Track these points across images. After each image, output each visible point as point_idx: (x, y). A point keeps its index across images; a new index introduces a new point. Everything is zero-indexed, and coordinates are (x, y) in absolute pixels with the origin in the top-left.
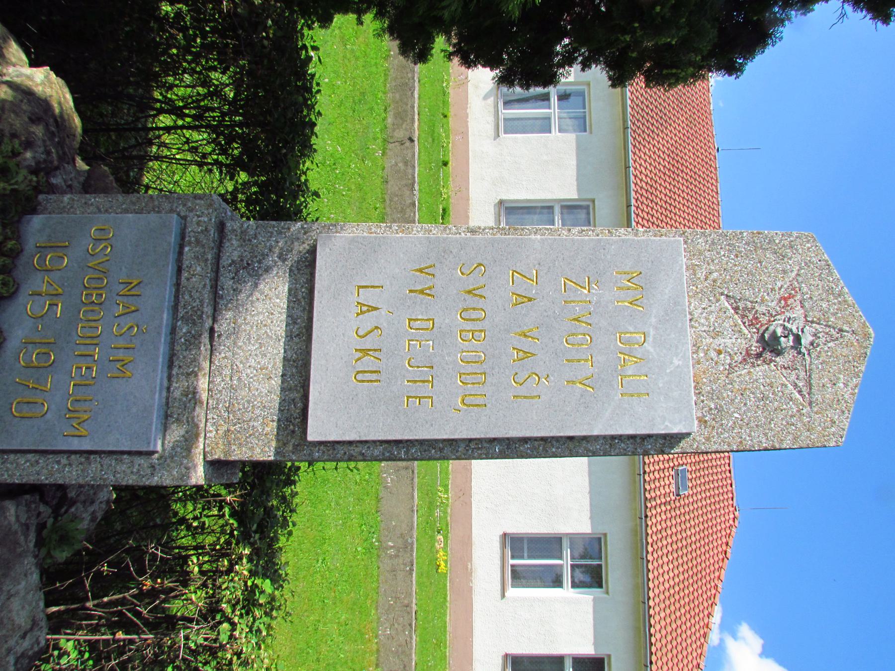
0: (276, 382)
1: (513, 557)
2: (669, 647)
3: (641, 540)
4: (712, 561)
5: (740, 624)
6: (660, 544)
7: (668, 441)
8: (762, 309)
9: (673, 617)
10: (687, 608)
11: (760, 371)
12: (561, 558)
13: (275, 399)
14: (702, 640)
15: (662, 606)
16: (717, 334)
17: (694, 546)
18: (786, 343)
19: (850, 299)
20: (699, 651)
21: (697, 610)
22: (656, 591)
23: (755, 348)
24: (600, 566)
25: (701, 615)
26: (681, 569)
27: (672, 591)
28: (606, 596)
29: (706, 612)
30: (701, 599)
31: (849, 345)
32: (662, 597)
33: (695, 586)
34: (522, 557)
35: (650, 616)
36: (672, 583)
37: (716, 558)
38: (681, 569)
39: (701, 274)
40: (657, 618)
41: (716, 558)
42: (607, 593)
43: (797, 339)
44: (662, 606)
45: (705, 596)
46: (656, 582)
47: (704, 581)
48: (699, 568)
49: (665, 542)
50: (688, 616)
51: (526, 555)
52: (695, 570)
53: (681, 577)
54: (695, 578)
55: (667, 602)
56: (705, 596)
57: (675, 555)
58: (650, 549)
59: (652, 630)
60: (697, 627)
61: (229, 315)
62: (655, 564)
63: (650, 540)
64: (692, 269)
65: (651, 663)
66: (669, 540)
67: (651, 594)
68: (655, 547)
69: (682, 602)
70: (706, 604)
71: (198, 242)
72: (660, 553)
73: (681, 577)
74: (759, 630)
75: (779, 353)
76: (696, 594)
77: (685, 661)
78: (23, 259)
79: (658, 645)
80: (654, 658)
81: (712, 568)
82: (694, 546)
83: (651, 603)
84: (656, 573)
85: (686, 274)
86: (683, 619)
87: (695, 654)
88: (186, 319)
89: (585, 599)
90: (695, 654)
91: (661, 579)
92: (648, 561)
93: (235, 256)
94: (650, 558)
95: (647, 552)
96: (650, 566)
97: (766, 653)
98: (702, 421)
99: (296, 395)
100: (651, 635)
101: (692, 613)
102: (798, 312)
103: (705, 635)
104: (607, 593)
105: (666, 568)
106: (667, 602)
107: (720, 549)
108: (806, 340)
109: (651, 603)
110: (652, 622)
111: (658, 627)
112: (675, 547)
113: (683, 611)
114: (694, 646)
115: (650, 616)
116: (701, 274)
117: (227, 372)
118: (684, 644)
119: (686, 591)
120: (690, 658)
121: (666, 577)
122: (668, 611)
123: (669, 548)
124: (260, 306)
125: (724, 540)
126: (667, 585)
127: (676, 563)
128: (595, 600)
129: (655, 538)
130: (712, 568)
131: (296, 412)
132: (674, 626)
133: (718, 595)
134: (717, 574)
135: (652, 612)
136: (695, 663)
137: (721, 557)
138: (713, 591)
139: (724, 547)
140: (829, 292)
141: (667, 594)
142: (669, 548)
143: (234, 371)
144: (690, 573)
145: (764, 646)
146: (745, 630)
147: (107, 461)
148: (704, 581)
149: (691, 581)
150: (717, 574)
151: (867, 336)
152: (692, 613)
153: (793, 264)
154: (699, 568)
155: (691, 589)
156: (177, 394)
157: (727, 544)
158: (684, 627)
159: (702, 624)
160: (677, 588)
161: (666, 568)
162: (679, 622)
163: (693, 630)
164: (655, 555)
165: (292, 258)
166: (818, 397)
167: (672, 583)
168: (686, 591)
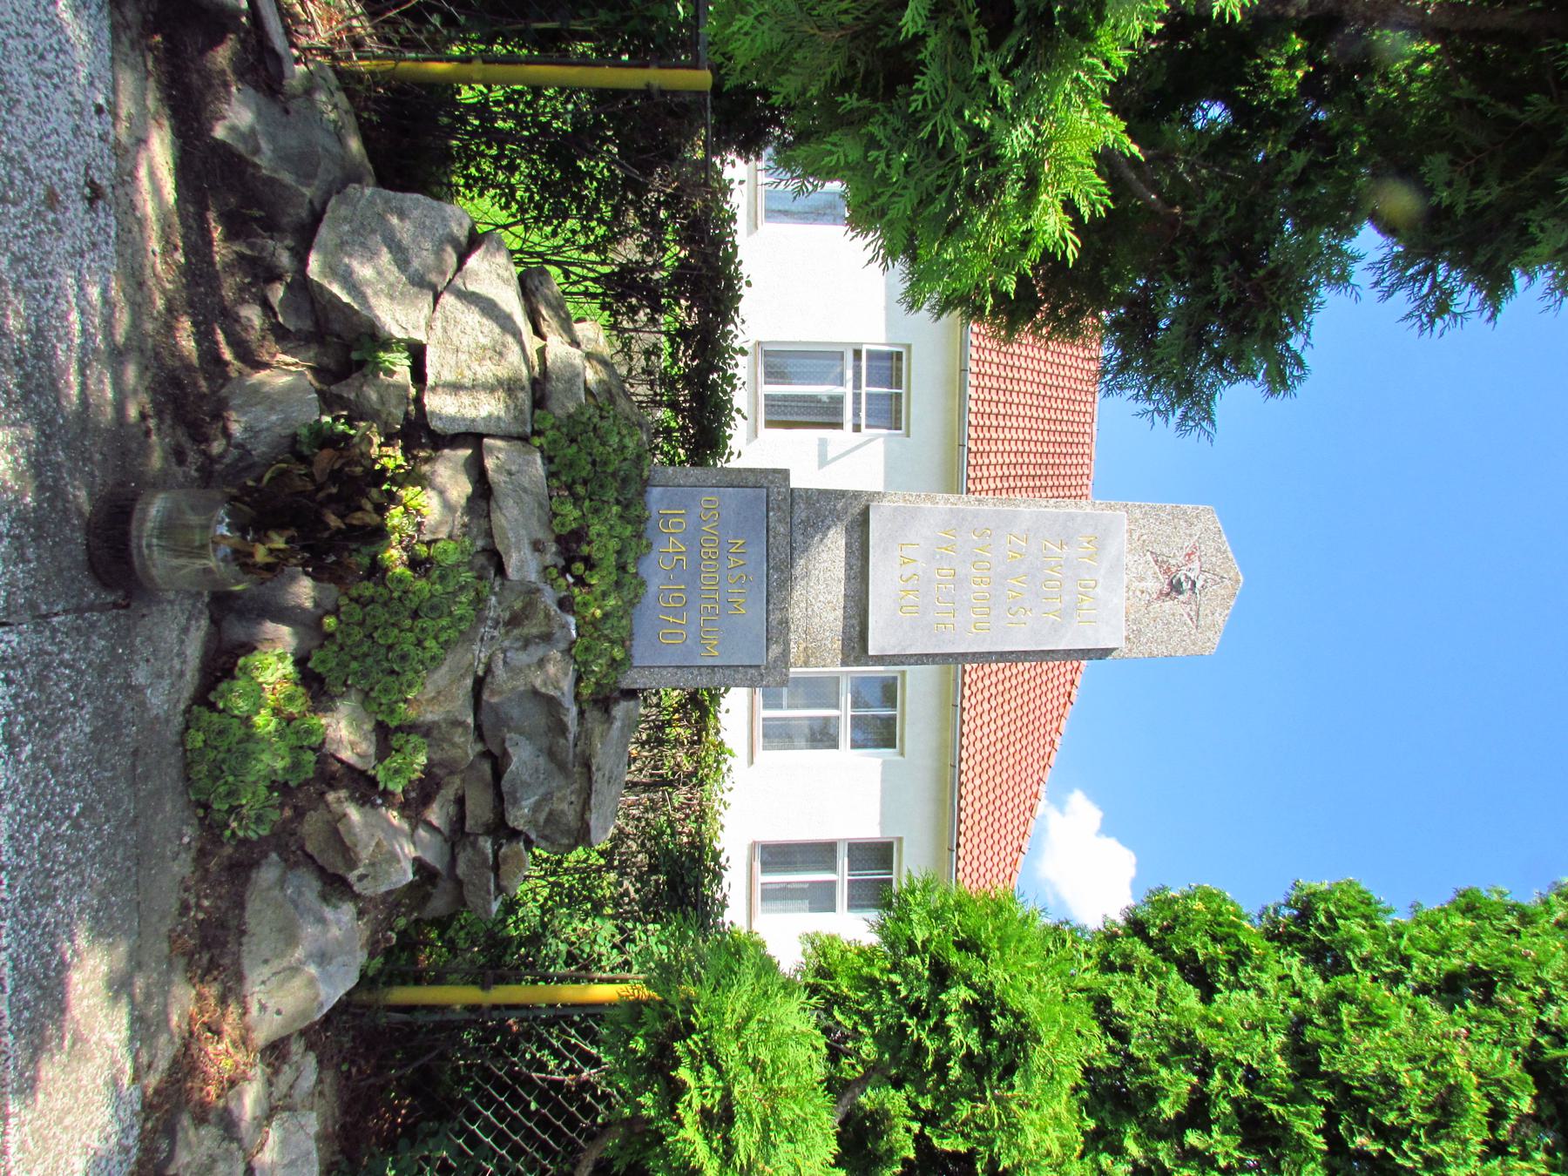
0: (840, 613)
1: (766, 707)
2: (983, 824)
3: (955, 680)
4: (1049, 707)
5: (1071, 791)
6: (980, 685)
7: (1104, 653)
8: (1173, 562)
9: (991, 784)
10: (1011, 772)
11: (1168, 604)
12: (837, 706)
13: (839, 625)
14: (1028, 814)
15: (978, 770)
16: (1142, 579)
17: (1026, 687)
18: (1186, 586)
19: (1231, 555)
20: (1022, 829)
21: (1024, 775)
22: (971, 750)
23: (1166, 589)
24: (893, 718)
25: (1029, 781)
26: (1006, 719)
27: (992, 750)
28: (899, 758)
29: (1036, 778)
30: (1030, 760)
31: (1226, 587)
32: (978, 758)
33: (1024, 742)
34: (780, 706)
35: (961, 784)
36: (993, 738)
37: (1056, 703)
38: (1006, 719)
39: (1135, 537)
40: (970, 786)
41: (1056, 703)
42: (902, 754)
43: (1194, 584)
44: (978, 770)
45: (1036, 756)
46: (972, 738)
47: (1036, 734)
48: (1031, 717)
49: (987, 682)
50: (1011, 783)
51: (862, 712)
52: (1025, 720)
53: (1006, 730)
54: (1025, 731)
55: (985, 765)
56: (1036, 756)
57: (1000, 700)
58: (967, 693)
59: (963, 803)
60: (1022, 797)
61: (802, 562)
62: (973, 713)
63: (967, 680)
64: (1131, 532)
65: (958, 845)
66: (994, 679)
67: (964, 755)
68: (974, 689)
69: (1005, 765)
70: (1036, 766)
71: (779, 508)
72: (980, 697)
73: (1006, 730)
74: (1095, 796)
75: (1180, 593)
76: (1024, 753)
77: (1003, 843)
78: (650, 524)
79: (969, 822)
80: (962, 840)
81: (1049, 717)
82: (1026, 687)
83: (964, 766)
84: (972, 725)
85: (1126, 536)
86: (1005, 787)
87: (1016, 833)
88: (777, 569)
89: (872, 761)
90: (1016, 833)
91: (979, 734)
92: (963, 709)
93: (804, 515)
94: (966, 704)
95: (963, 696)
96: (966, 717)
97: (1107, 829)
98: (1127, 638)
99: (855, 622)
100: (960, 809)
101: (1017, 779)
102: (1196, 565)
103: (1031, 809)
104: (902, 754)
105: (986, 718)
106: (985, 765)
107: (1062, 690)
108: (1198, 585)
109: (964, 766)
110: (963, 792)
111: (970, 798)
112: (1000, 688)
113: (1005, 776)
114: (1016, 822)
115: (961, 784)
116: (1135, 537)
117: (803, 605)
118: (1003, 821)
119: (1012, 750)
120: (1009, 838)
121: (986, 730)
122: (985, 777)
123: (993, 690)
124: (824, 555)
125: (1069, 677)
126: (986, 742)
127: (1000, 711)
128: (885, 764)
129: (974, 676)
130: (1049, 717)
131: (855, 633)
132: (992, 796)
133: (1054, 754)
134: (1055, 724)
135: (963, 778)
136: (1015, 844)
137: (1062, 701)
138: (1048, 749)
139: (1068, 687)
140: (1218, 550)
141: (985, 754)
142: (993, 690)
143: (809, 605)
144: (1019, 724)
145: (1103, 821)
146: (1078, 799)
147: (727, 672)
148: (1036, 734)
149: (1019, 735)
150: (1055, 724)
151: (1237, 581)
152: (1017, 779)
153: (1196, 530)
154: (1031, 717)
155: (1018, 746)
156: (774, 623)
157: (1072, 683)
158: (1004, 798)
159: (1029, 793)
160: (999, 746)
161: (986, 718)
162: (998, 792)
163: (1017, 801)
164: (973, 701)
165: (847, 519)
166: (1202, 623)
167: (993, 738)
168: (1012, 750)
